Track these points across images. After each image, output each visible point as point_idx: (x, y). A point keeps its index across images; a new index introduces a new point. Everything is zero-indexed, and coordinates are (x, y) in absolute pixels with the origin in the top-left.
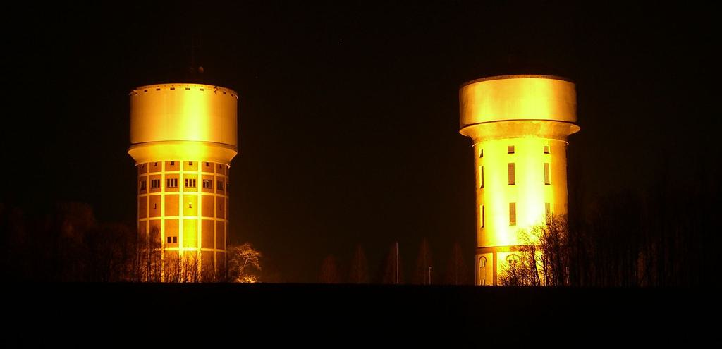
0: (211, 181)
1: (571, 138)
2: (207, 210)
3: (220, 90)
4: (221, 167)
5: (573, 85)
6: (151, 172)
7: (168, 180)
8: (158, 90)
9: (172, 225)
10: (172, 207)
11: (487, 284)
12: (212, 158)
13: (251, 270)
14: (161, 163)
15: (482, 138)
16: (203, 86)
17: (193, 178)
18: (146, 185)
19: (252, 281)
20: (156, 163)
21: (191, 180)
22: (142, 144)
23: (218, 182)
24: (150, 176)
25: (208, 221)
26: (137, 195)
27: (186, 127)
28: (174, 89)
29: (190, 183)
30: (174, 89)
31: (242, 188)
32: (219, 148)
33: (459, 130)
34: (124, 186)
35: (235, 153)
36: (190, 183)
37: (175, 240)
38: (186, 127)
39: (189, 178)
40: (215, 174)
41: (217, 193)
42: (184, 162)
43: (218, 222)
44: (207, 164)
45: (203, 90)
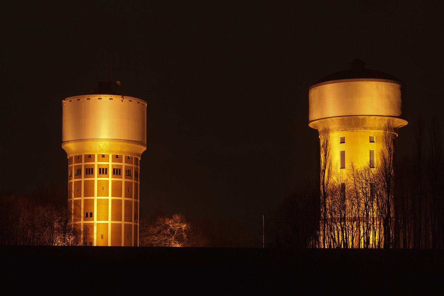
0: (120, 170)
1: (399, 130)
2: (116, 192)
3: (126, 99)
4: (129, 158)
5: (397, 86)
6: (85, 162)
7: (87, 169)
8: (99, 99)
9: (89, 204)
10: (89, 191)
11: (109, 246)
12: (120, 152)
13: (179, 239)
14: (94, 155)
15: (332, 130)
16: (113, 96)
17: (105, 167)
18: (72, 175)
19: (178, 246)
20: (78, 156)
21: (103, 169)
22: (87, 140)
23: (126, 171)
24: (85, 166)
25: (117, 200)
26: (68, 181)
27: (104, 128)
28: (101, 99)
29: (103, 171)
30: (101, 99)
31: (152, 176)
32: (126, 144)
33: (308, 123)
34: (54, 176)
35: (144, 149)
36: (103, 171)
37: (92, 215)
38: (104, 128)
39: (102, 167)
40: (124, 164)
41: (125, 178)
42: (98, 155)
43: (126, 201)
44: (117, 156)
45: (112, 99)
